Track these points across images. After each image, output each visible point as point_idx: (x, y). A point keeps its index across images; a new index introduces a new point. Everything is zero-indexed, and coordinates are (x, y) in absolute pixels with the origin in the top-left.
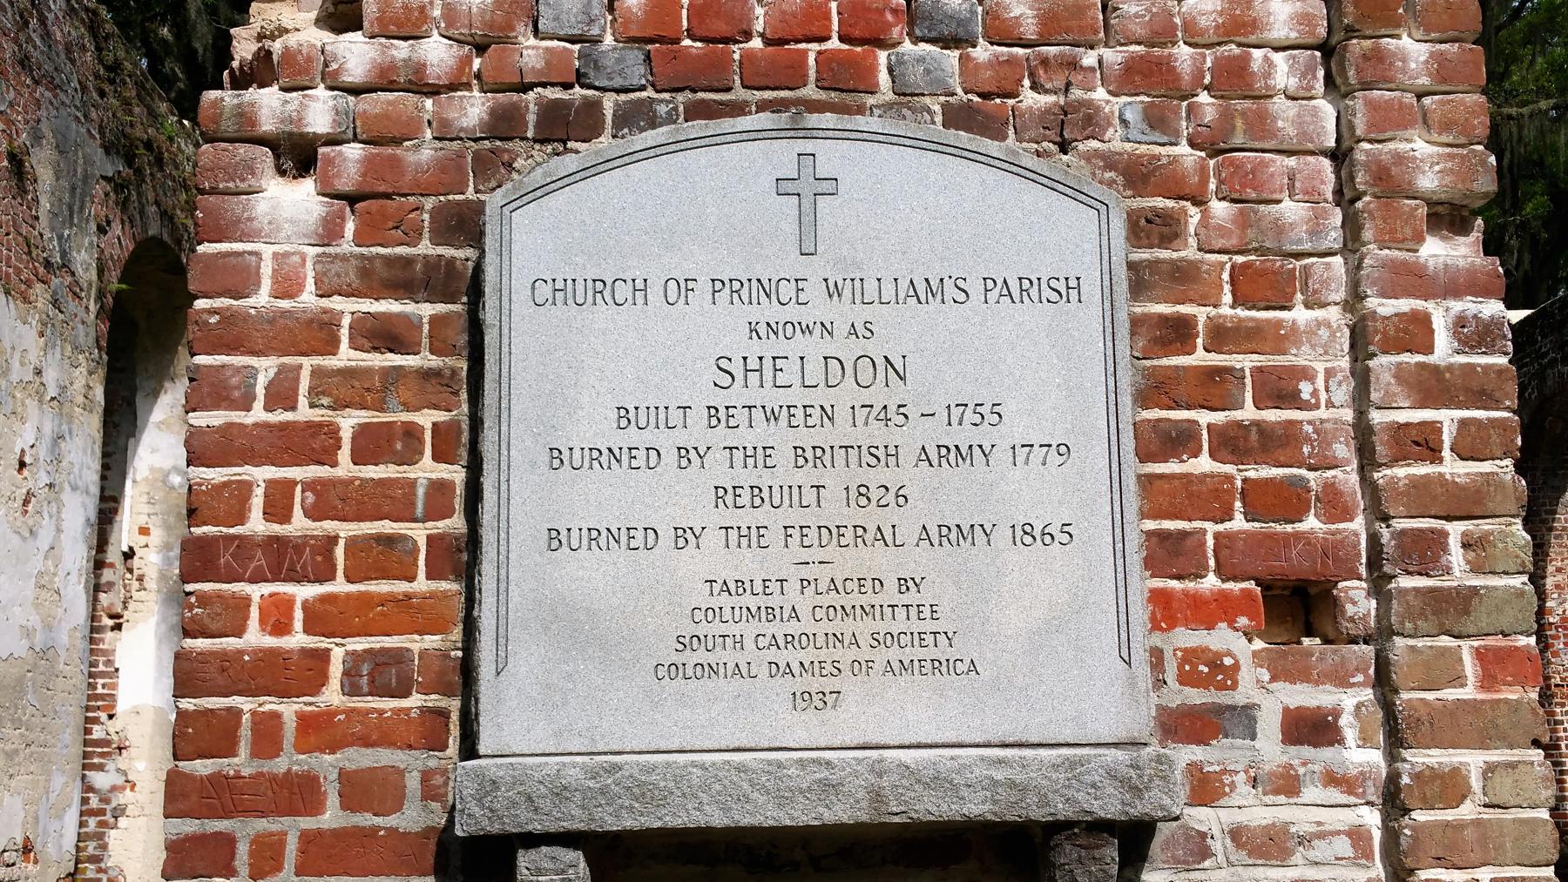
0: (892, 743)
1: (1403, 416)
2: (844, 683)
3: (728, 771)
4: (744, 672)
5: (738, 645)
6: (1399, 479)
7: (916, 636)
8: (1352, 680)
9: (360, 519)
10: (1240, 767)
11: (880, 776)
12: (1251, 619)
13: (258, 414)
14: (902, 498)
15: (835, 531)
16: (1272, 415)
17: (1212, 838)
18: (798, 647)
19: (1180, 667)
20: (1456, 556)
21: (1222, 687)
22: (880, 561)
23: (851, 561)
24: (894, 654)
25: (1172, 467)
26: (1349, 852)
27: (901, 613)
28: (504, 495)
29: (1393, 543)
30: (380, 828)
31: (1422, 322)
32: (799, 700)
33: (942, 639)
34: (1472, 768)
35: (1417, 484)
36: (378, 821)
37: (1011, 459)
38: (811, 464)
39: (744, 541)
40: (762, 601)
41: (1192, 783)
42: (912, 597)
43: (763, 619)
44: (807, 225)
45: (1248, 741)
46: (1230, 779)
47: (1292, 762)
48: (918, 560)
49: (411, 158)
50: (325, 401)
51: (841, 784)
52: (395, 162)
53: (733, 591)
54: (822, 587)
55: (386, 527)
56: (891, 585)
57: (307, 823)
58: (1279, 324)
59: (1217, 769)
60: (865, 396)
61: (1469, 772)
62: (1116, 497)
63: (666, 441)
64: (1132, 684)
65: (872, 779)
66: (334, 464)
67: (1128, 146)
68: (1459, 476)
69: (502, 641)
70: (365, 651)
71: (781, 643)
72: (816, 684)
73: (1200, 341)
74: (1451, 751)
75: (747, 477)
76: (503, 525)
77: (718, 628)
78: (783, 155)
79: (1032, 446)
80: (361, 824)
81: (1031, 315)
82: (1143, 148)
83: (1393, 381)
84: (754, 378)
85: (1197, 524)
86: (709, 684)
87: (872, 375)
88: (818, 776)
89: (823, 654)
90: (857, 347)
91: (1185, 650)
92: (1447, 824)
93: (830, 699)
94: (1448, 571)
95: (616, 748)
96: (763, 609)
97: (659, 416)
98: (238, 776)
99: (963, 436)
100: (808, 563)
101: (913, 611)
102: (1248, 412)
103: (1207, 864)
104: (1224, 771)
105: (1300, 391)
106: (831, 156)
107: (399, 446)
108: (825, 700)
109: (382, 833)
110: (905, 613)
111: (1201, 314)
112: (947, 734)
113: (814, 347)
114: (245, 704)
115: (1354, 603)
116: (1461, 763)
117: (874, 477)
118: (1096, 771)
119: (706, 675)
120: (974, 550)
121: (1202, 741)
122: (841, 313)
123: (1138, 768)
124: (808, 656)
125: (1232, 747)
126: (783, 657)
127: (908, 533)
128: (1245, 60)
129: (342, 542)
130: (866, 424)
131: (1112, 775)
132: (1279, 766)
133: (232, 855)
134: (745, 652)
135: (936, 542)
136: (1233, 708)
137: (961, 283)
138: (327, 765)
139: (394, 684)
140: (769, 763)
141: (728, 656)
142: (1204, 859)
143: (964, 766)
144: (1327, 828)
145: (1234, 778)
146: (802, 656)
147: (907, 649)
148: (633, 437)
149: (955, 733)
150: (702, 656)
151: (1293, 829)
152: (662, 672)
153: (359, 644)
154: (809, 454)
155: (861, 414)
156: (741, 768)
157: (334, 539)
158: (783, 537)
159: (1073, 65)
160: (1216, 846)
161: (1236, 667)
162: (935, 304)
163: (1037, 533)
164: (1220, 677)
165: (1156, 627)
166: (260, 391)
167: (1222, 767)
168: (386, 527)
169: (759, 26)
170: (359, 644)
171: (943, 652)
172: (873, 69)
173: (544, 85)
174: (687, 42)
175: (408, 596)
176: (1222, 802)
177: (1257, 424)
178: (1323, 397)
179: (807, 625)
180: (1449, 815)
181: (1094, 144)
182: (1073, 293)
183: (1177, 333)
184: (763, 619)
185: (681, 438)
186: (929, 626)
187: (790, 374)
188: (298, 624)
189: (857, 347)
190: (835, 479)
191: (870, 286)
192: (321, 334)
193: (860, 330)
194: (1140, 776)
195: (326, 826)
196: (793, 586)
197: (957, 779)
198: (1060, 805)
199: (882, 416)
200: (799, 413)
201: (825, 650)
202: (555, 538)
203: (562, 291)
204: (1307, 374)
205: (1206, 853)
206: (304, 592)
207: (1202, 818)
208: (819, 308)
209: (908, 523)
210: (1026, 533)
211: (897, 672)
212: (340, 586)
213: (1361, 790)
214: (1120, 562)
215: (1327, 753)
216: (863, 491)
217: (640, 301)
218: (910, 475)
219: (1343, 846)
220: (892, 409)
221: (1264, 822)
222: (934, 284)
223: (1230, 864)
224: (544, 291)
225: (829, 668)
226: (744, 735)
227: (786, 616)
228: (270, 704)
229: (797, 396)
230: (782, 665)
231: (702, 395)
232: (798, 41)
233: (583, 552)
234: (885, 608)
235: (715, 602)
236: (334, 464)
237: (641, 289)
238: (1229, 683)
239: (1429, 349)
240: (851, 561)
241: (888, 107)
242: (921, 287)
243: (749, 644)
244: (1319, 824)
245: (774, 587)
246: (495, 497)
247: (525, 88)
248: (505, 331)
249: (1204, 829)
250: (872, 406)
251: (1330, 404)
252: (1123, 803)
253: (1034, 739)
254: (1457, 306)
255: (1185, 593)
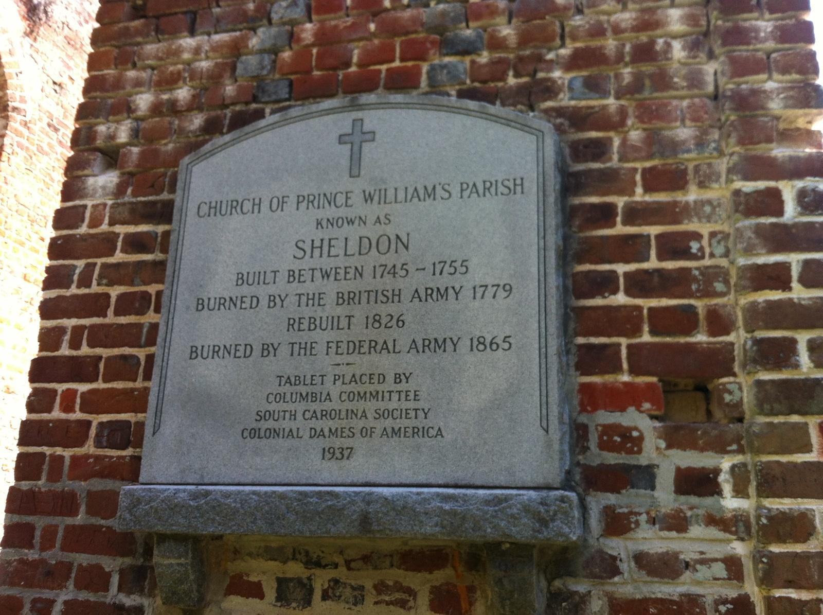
0: (383, 482)
1: (761, 260)
2: (358, 443)
3: (274, 498)
4: (295, 434)
5: (293, 417)
6: (759, 303)
7: (404, 412)
8: (729, 448)
9: (113, 346)
10: (643, 510)
11: (368, 503)
12: (653, 405)
13: (74, 290)
14: (401, 322)
15: (357, 344)
16: (670, 265)
17: (621, 560)
18: (329, 418)
19: (600, 437)
20: (804, 358)
21: (630, 452)
22: (385, 363)
23: (363, 363)
24: (388, 423)
25: (598, 302)
26: (724, 574)
27: (395, 397)
28: (170, 327)
29: (755, 348)
30: (103, 527)
31: (776, 195)
32: (327, 453)
33: (421, 413)
34: (816, 513)
35: (772, 305)
36: (103, 522)
37: (472, 295)
38: (346, 302)
39: (302, 351)
40: (310, 389)
41: (606, 520)
42: (403, 386)
43: (310, 400)
44: (355, 161)
45: (648, 491)
46: (635, 519)
47: (682, 507)
48: (408, 361)
49: (163, 149)
50: (104, 281)
51: (343, 509)
52: (156, 153)
53: (293, 383)
54: (347, 380)
55: (127, 351)
56: (390, 378)
57: (69, 521)
58: (675, 204)
59: (626, 510)
60: (383, 259)
61: (814, 516)
62: (543, 317)
63: (263, 292)
64: (549, 445)
65: (363, 505)
66: (105, 316)
67: (573, 103)
68: (804, 299)
69: (159, 414)
70: (108, 422)
71: (319, 416)
72: (338, 442)
73: (619, 219)
74: (800, 500)
75: (307, 312)
76: (167, 344)
77: (282, 406)
78: (344, 122)
79: (486, 286)
80: (95, 523)
81: (490, 204)
82: (583, 103)
83: (753, 236)
84: (317, 252)
85: (615, 340)
86: (272, 441)
87: (387, 247)
88: (329, 503)
89: (344, 423)
90: (380, 229)
91: (604, 426)
92: (796, 555)
93: (346, 453)
94: (797, 366)
95: (214, 481)
96: (310, 394)
97: (260, 278)
98: (40, 492)
99: (442, 282)
100: (339, 365)
101: (403, 395)
102: (653, 263)
103: (616, 579)
104: (631, 513)
105: (691, 248)
106: (372, 119)
107: (137, 305)
108: (345, 454)
109: (104, 529)
110: (398, 396)
111: (620, 202)
112: (420, 477)
113: (354, 233)
114: (47, 450)
115: (730, 393)
116: (807, 509)
117: (384, 310)
118: (516, 506)
119: (272, 436)
120: (445, 355)
121: (615, 490)
122: (372, 211)
123: (546, 505)
124: (334, 424)
125: (637, 495)
126: (318, 424)
127: (404, 343)
128: (652, 43)
129: (103, 360)
130: (382, 277)
131: (526, 509)
132: (672, 510)
133: (33, 537)
134: (297, 421)
135: (421, 350)
136: (638, 467)
137: (446, 187)
138: (81, 487)
139: (118, 442)
140: (301, 493)
141: (286, 424)
142: (614, 576)
143: (425, 500)
144: (708, 556)
145: (638, 518)
146: (331, 423)
147: (398, 420)
148: (245, 290)
149: (425, 477)
150: (271, 424)
151: (682, 557)
152: (246, 434)
153: (105, 418)
154: (346, 297)
155: (379, 271)
156: (283, 496)
157: (100, 358)
158: (326, 348)
159: (539, 59)
160: (624, 567)
161: (641, 438)
162: (429, 201)
163: (488, 343)
164: (629, 445)
165: (583, 410)
166: (76, 277)
167: (629, 509)
168: (127, 351)
169: (355, 59)
170: (105, 418)
171: (420, 422)
172: (419, 74)
173: (233, 104)
174: (316, 73)
175: (133, 390)
176: (628, 535)
177: (658, 271)
178: (707, 251)
179: (335, 405)
180: (799, 548)
181: (549, 104)
182: (519, 189)
183: (606, 214)
184: (310, 400)
185: (272, 289)
186: (411, 405)
187: (338, 250)
188: (77, 407)
189: (380, 229)
190: (359, 312)
191: (390, 194)
192: (107, 244)
193: (382, 219)
194: (547, 511)
195: (77, 523)
196: (329, 379)
197: (419, 508)
198: (489, 530)
199: (392, 271)
200: (342, 272)
201: (345, 421)
202: (194, 353)
203: (215, 209)
204: (697, 236)
205: (616, 571)
206: (83, 387)
207: (616, 546)
208: (359, 208)
209: (403, 338)
210: (480, 343)
211: (390, 435)
212: (100, 385)
213: (734, 529)
214: (543, 361)
215: (708, 501)
216: (377, 319)
217: (256, 210)
218: (409, 309)
219: (720, 570)
220: (399, 266)
221: (660, 551)
222: (430, 189)
223: (635, 581)
224: (205, 209)
225: (347, 432)
226: (291, 475)
227: (323, 399)
228: (59, 451)
229: (341, 262)
230: (318, 430)
231: (286, 263)
232: (375, 64)
233: (210, 359)
234: (385, 394)
235: (282, 390)
236: (105, 316)
237: (257, 205)
238: (635, 449)
239: (780, 212)
240: (363, 363)
241: (426, 94)
242: (421, 192)
243: (299, 416)
244: (702, 553)
245: (318, 380)
246: (165, 328)
247: (226, 106)
248: (181, 233)
249: (615, 554)
250: (386, 266)
251: (712, 255)
252: (533, 530)
253: (479, 483)
254: (800, 184)
255: (604, 385)
